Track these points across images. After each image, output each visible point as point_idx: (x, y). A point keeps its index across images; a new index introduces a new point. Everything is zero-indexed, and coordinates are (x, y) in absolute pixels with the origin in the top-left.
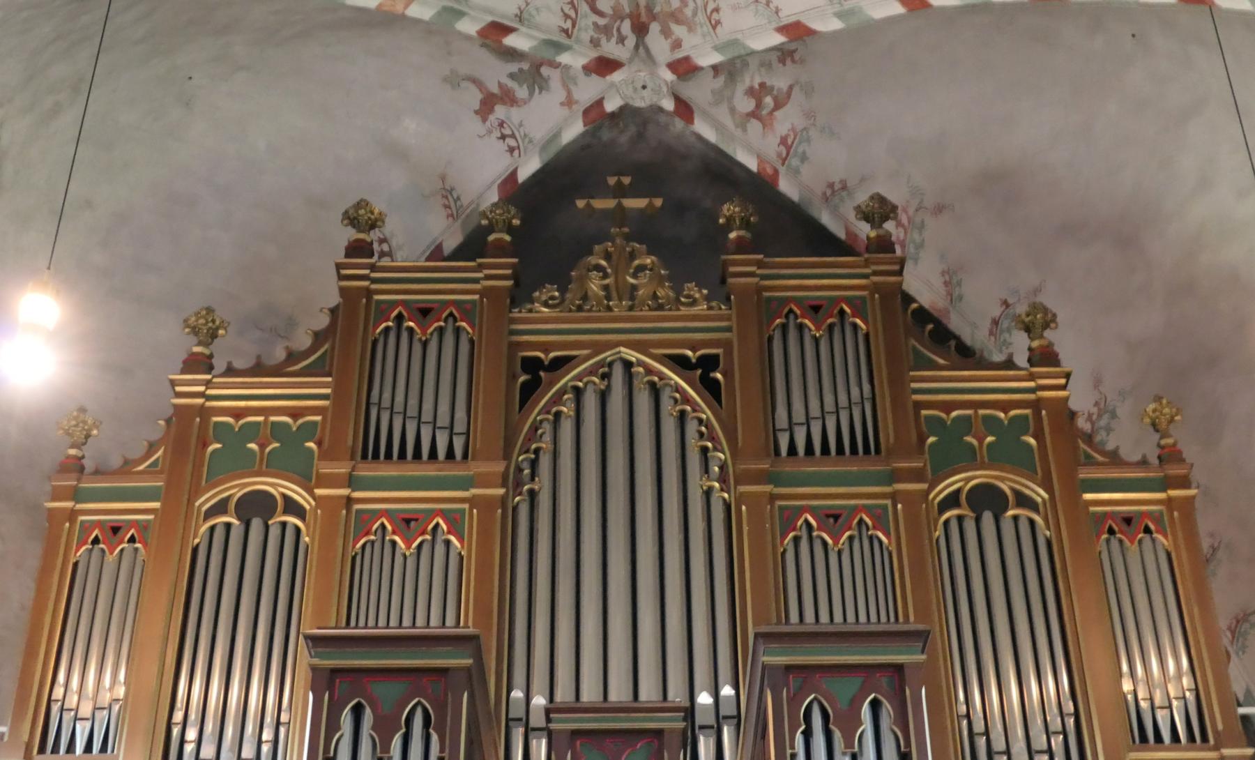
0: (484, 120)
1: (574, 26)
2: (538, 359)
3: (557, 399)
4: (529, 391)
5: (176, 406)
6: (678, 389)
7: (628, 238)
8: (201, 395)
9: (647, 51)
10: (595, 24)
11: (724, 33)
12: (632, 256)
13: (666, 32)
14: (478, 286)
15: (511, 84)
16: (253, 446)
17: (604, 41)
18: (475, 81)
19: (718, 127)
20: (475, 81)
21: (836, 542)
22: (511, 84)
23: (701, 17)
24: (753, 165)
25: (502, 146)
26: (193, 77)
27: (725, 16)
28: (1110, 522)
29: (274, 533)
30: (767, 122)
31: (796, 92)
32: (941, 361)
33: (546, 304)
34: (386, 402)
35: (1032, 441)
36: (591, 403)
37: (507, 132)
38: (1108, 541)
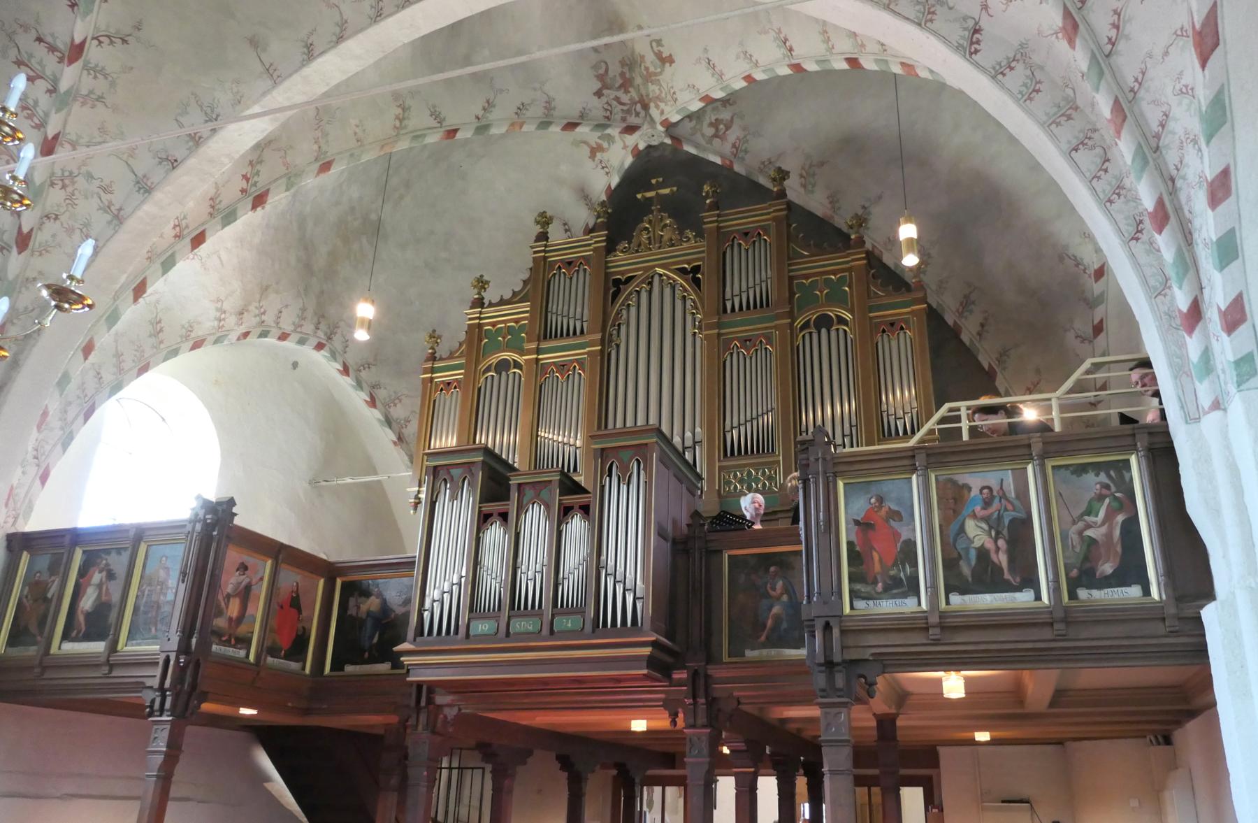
0: (594, 160)
1: (611, 114)
2: (620, 279)
3: (627, 298)
4: (615, 295)
5: (469, 325)
6: (682, 285)
7: (659, 211)
8: (717, 221)
9: (650, 116)
10: (622, 110)
11: (679, 104)
12: (662, 220)
13: (657, 107)
14: (591, 248)
15: (600, 141)
16: (500, 338)
17: (628, 118)
18: (585, 142)
19: (697, 146)
20: (585, 142)
21: (748, 354)
22: (600, 141)
23: (669, 97)
24: (718, 161)
25: (603, 172)
26: (295, 359)
27: (678, 95)
28: (883, 326)
29: (511, 377)
30: (722, 138)
31: (735, 119)
32: (806, 253)
33: (622, 252)
34: (554, 310)
35: (847, 289)
36: (644, 296)
37: (604, 165)
38: (882, 336)
